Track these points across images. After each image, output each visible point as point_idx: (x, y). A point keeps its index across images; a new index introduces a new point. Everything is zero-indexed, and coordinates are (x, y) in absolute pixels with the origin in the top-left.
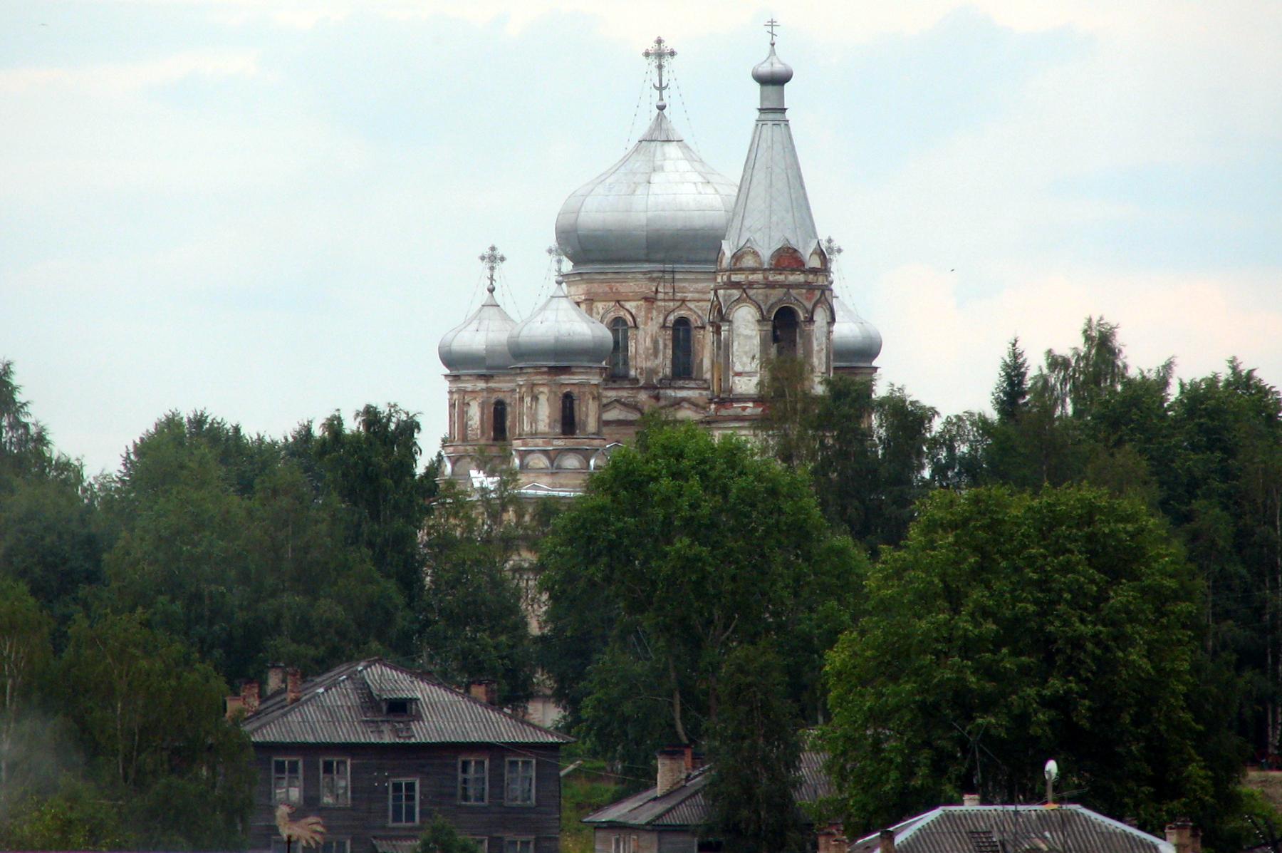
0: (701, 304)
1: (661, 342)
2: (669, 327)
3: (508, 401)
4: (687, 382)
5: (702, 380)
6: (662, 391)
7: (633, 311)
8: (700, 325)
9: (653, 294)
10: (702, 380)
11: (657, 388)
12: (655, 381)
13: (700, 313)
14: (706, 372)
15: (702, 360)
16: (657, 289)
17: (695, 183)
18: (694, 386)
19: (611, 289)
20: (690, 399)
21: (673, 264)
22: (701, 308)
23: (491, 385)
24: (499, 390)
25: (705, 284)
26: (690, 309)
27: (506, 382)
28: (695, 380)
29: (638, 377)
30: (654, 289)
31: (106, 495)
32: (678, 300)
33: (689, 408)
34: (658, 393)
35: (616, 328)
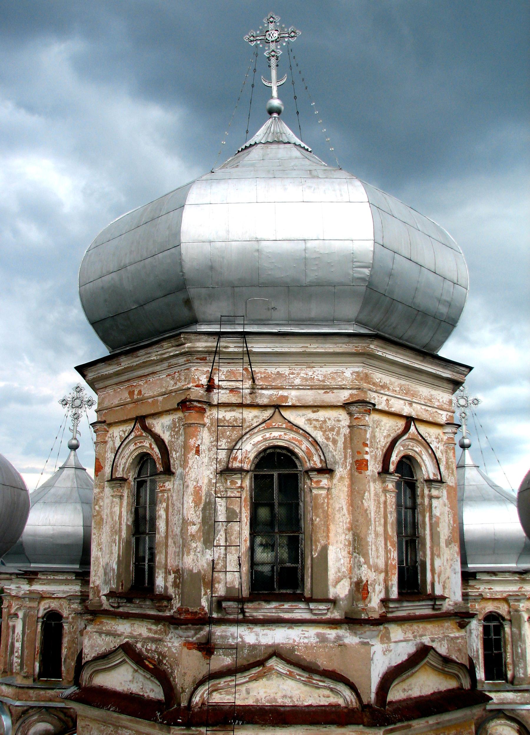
0: (322, 414)
1: (221, 506)
2: (240, 471)
3: (65, 613)
4: (286, 606)
5: (327, 600)
6: (218, 631)
7: (166, 437)
8: (319, 465)
9: (201, 392)
10: (327, 600)
11: (211, 621)
12: (204, 603)
13: (319, 436)
14: (338, 581)
15: (325, 550)
16: (211, 380)
17: (310, 170)
18: (307, 616)
19: (131, 393)
20: (292, 649)
21: (244, 332)
22: (322, 426)
23: (37, 587)
24: (50, 597)
25: (329, 370)
26: (294, 427)
27: (133, 568)
28: (309, 600)
29: (171, 591)
30: (204, 380)
31: (390, 536)
32: (264, 407)
33: (290, 675)
34: (210, 634)
35: (266, 472)
